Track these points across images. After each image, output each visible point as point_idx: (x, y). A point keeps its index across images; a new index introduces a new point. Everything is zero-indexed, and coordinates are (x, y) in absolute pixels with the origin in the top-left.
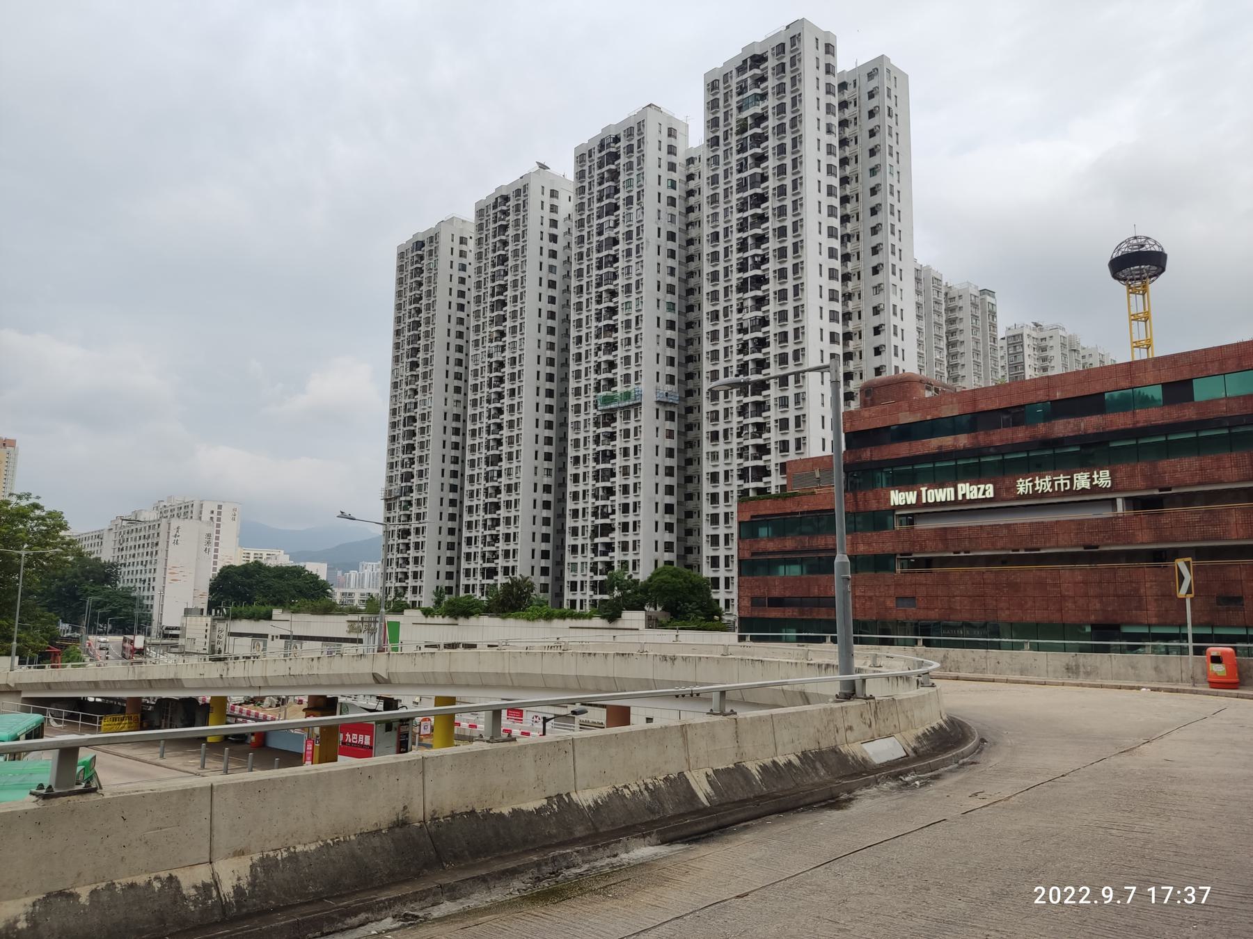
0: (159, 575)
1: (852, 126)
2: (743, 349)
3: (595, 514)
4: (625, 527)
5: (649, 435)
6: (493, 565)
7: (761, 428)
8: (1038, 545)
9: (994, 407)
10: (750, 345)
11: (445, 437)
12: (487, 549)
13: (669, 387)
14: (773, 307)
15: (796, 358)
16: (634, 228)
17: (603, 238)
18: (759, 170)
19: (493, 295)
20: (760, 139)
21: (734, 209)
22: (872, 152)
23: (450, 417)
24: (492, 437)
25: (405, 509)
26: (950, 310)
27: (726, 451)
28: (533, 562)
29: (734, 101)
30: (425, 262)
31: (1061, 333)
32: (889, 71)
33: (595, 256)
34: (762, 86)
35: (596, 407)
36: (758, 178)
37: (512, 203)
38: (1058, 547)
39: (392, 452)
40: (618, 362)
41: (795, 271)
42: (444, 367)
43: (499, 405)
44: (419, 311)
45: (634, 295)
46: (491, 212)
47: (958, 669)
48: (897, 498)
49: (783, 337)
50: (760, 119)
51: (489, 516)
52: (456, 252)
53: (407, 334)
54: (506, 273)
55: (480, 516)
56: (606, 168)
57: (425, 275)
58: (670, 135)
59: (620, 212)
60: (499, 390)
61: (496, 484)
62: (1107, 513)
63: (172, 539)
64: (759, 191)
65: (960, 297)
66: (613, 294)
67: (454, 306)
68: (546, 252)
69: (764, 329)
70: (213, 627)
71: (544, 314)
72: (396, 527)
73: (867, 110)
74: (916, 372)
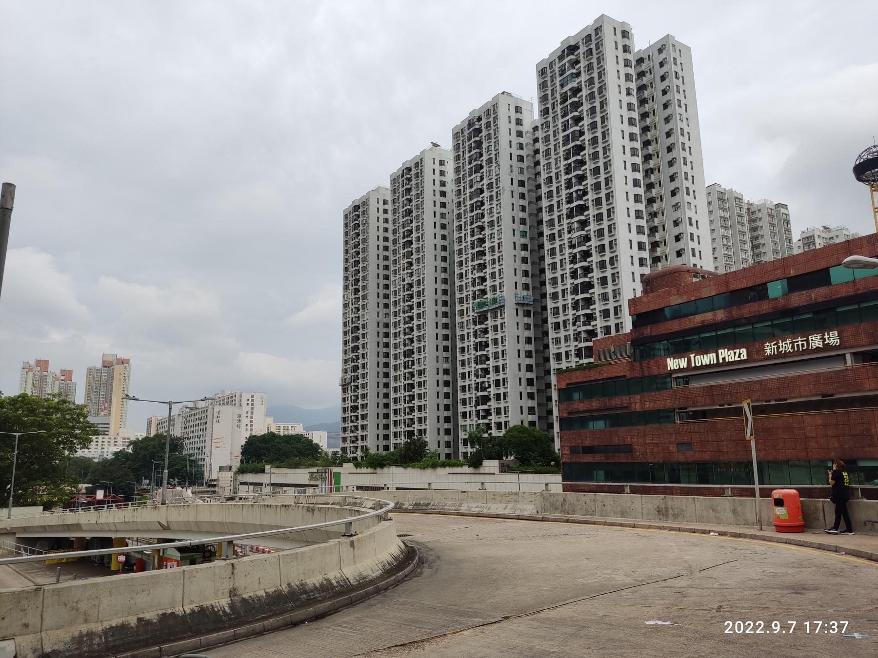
0: (207, 444)
1: (649, 89)
2: (573, 260)
3: (477, 389)
4: (498, 397)
5: (512, 329)
6: (411, 429)
7: (590, 318)
8: (785, 396)
9: (740, 287)
10: (578, 256)
11: (378, 339)
12: (407, 417)
13: (525, 293)
14: (593, 227)
15: (612, 263)
16: (494, 180)
17: (473, 189)
18: (578, 128)
19: (403, 238)
20: (577, 105)
21: (562, 158)
22: (666, 106)
23: (381, 325)
24: (407, 337)
25: (355, 391)
26: (751, 221)
27: (566, 336)
28: (439, 426)
29: (558, 80)
30: (361, 219)
31: (845, 232)
32: (674, 46)
33: (469, 203)
34: (577, 67)
35: (473, 310)
36: (577, 134)
37: (413, 172)
38: (801, 397)
39: (345, 352)
40: (487, 277)
41: (608, 199)
42: (434, 297)
43: (410, 314)
44: (358, 253)
45: (496, 228)
46: (401, 180)
47: (574, 512)
48: (672, 364)
49: (602, 249)
50: (576, 91)
51: (407, 393)
52: (381, 211)
53: (351, 270)
54: (412, 222)
55: (402, 394)
56: (473, 140)
57: (361, 228)
58: (517, 112)
59: (484, 170)
60: (410, 303)
61: (411, 370)
62: (838, 367)
63: (215, 419)
64: (578, 143)
65: (759, 210)
66: (482, 228)
67: (381, 248)
68: (438, 204)
69: (588, 244)
70: (235, 479)
71: (439, 248)
72: (349, 404)
73: (658, 79)
74: (712, 270)
